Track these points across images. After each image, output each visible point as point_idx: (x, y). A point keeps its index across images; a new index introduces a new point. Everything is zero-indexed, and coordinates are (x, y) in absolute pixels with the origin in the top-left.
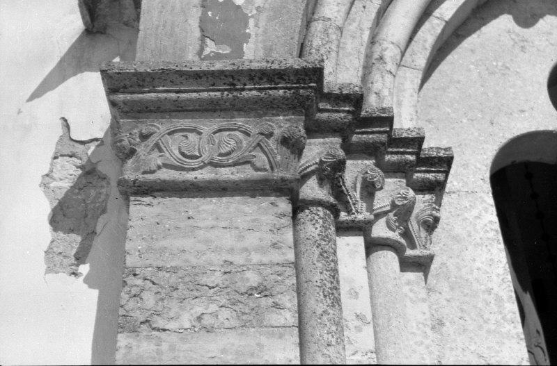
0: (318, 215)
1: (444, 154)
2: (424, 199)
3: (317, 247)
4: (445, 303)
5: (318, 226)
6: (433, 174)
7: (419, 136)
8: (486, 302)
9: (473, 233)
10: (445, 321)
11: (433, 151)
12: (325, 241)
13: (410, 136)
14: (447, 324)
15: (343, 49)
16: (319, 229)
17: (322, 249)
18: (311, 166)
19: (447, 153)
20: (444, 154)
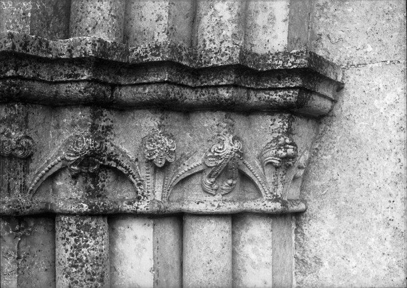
0: (70, 231)
1: (293, 64)
2: (273, 127)
3: (67, 277)
4: (327, 236)
5: (68, 247)
6: (281, 93)
7: (231, 62)
8: (380, 237)
9: (381, 132)
10: (323, 260)
11: (278, 60)
12: (76, 267)
13: (220, 64)
14: (326, 264)
15: (25, 45)
16: (70, 251)
17: (72, 279)
18: (156, 83)
19: (298, 61)
20: (293, 64)
